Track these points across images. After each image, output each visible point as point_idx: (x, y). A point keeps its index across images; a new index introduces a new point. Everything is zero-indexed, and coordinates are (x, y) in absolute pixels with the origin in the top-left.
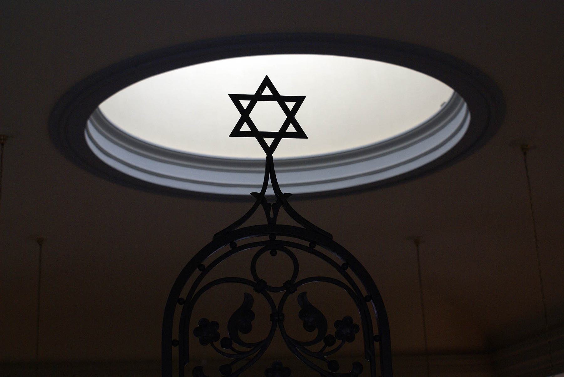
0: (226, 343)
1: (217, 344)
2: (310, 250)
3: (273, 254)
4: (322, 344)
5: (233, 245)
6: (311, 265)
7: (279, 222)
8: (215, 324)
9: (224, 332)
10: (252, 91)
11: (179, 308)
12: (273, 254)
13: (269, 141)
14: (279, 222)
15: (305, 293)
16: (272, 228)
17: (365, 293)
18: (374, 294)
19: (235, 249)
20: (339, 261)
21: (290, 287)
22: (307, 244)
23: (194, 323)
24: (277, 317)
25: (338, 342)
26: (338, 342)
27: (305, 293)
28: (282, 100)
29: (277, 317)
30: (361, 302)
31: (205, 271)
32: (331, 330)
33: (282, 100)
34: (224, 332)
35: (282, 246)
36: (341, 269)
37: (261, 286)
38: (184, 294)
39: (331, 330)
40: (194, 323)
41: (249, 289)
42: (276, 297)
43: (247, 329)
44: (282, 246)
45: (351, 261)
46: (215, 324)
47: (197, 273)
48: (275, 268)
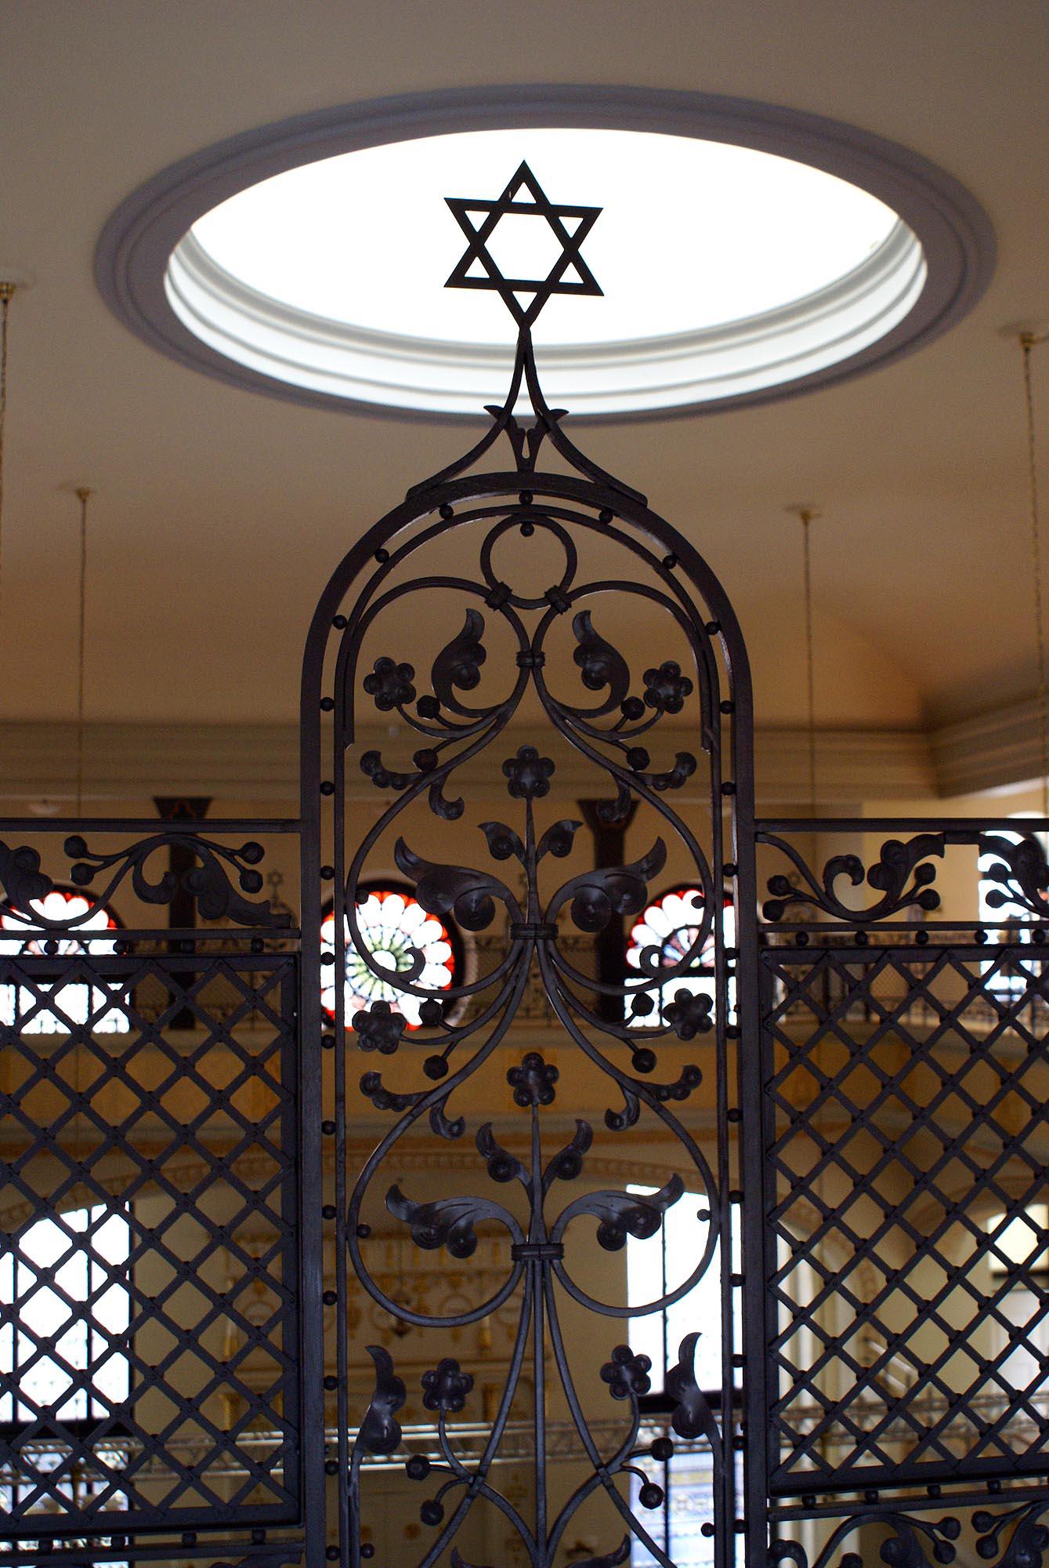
0: (428, 707)
1: (411, 709)
2: (601, 526)
3: (527, 531)
4: (617, 714)
5: (447, 513)
6: (601, 557)
7: (540, 467)
8: (407, 670)
9: (424, 686)
10: (494, 195)
11: (335, 637)
12: (527, 531)
13: (525, 299)
14: (540, 467)
15: (587, 613)
16: (525, 479)
17: (707, 616)
18: (726, 621)
19: (451, 519)
20: (660, 550)
21: (558, 599)
22: (594, 513)
23: (365, 667)
24: (531, 659)
25: (650, 712)
26: (650, 712)
27: (587, 613)
28: (553, 214)
29: (531, 659)
30: (699, 634)
31: (388, 562)
32: (637, 689)
33: (553, 214)
34: (424, 686)
35: (544, 517)
36: (663, 568)
37: (499, 596)
38: (345, 609)
39: (637, 689)
40: (365, 667)
41: (478, 603)
42: (531, 619)
43: (470, 681)
44: (544, 517)
45: (682, 553)
46: (407, 670)
47: (373, 565)
48: (530, 562)
